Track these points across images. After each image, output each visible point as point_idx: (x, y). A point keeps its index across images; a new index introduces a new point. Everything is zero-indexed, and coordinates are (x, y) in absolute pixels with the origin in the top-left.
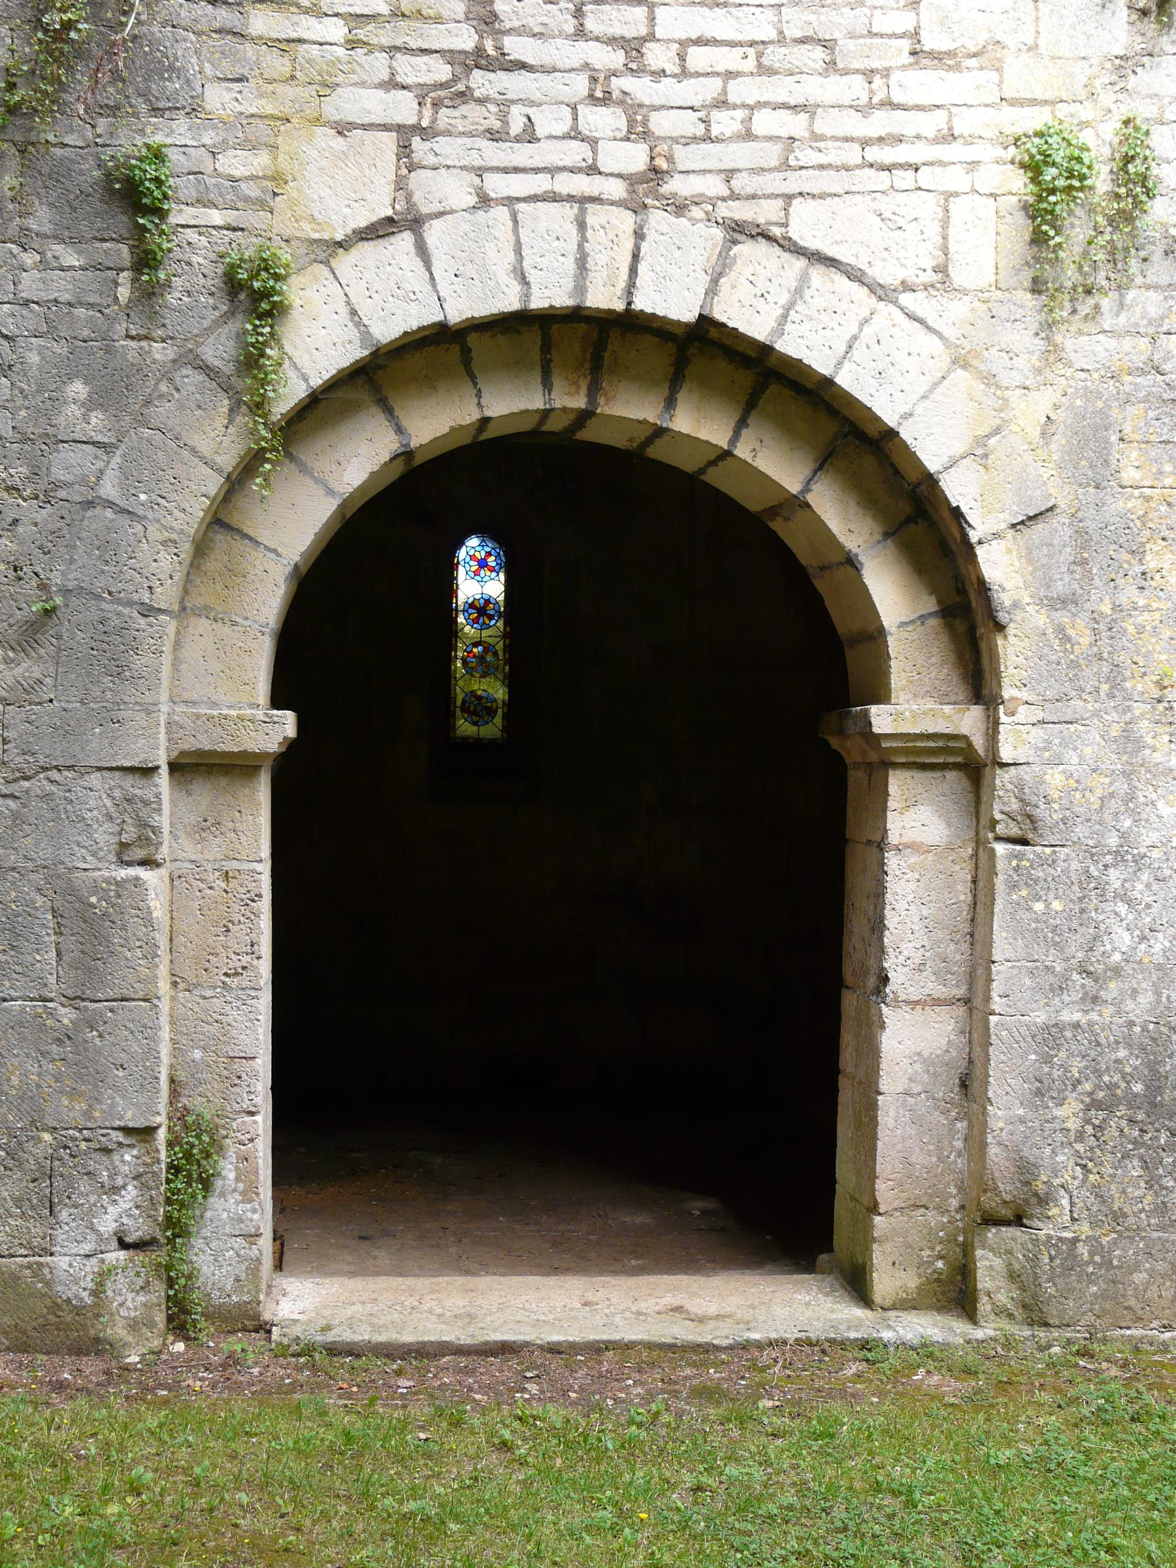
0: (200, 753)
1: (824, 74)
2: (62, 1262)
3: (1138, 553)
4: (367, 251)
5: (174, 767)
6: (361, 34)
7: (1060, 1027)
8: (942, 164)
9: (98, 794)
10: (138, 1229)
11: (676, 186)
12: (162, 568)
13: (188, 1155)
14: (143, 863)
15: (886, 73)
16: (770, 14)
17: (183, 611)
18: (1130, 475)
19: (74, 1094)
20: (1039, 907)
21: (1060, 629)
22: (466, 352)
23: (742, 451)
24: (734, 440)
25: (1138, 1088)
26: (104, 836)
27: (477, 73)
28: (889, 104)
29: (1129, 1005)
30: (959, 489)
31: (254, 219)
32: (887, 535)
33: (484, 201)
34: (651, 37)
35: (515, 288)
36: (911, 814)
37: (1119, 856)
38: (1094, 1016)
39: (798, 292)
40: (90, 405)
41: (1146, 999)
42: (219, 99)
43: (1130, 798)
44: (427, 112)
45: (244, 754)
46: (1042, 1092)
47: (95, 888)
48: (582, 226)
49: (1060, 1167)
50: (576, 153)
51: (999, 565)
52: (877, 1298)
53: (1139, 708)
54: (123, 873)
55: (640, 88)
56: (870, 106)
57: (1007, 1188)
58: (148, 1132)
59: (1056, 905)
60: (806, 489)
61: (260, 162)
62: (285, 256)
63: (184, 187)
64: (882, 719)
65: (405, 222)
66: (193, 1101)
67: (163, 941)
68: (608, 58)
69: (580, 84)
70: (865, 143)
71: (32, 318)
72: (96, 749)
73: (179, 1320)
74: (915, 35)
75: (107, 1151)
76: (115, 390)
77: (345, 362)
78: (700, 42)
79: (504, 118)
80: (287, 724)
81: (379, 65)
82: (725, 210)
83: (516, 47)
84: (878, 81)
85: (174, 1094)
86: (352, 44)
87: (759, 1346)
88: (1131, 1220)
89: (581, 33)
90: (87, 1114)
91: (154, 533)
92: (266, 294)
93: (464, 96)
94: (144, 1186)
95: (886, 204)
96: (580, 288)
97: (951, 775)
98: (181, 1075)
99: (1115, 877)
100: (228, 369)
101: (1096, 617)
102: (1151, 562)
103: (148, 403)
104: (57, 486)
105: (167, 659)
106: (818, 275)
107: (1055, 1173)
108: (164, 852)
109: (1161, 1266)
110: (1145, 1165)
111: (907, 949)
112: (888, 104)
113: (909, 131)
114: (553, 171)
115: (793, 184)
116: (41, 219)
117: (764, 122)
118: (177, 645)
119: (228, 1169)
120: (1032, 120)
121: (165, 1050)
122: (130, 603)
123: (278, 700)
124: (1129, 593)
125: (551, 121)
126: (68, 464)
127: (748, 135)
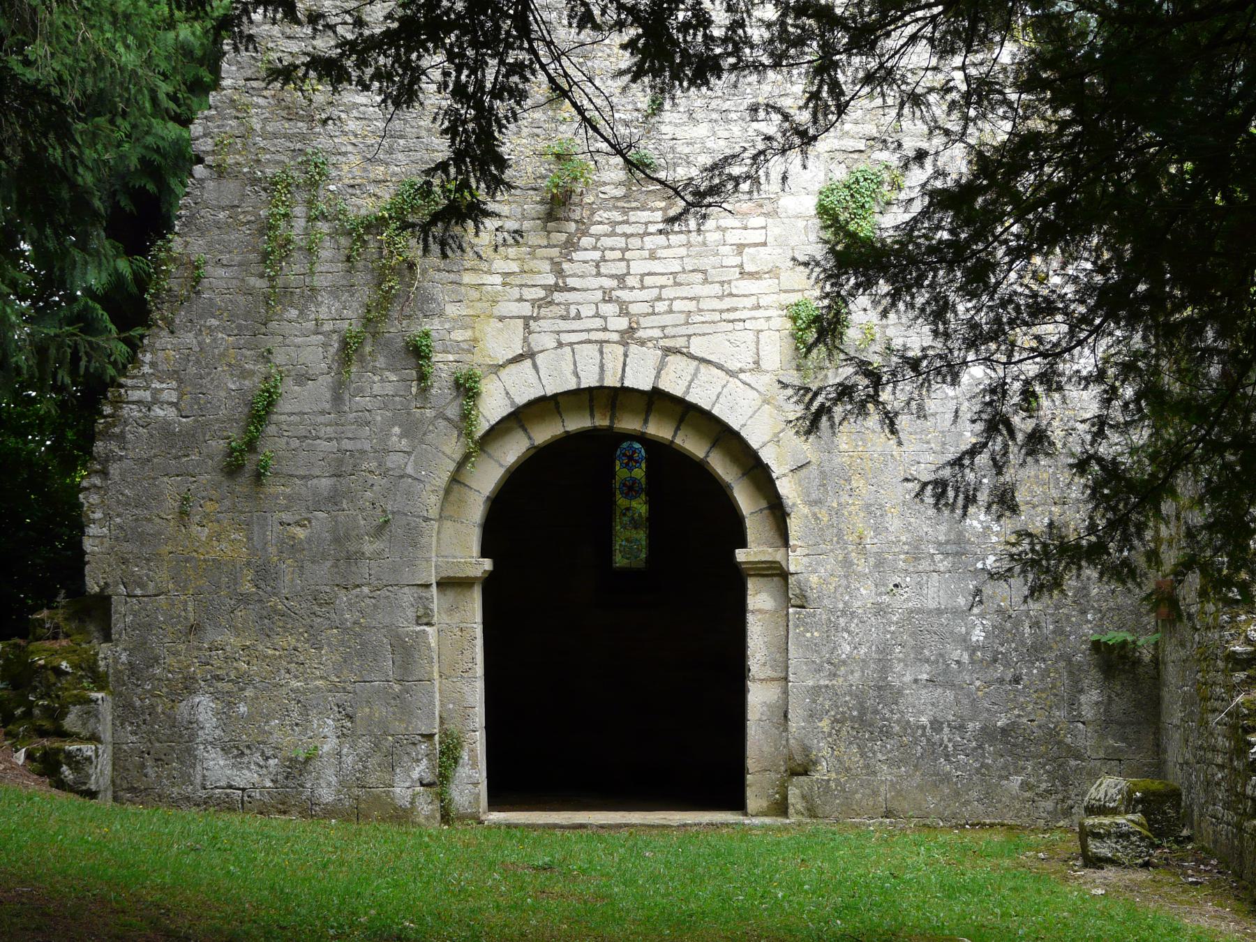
0: (449, 578)
1: (703, 284)
2: (398, 790)
3: (849, 481)
5: (438, 584)
6: (508, 280)
7: (820, 687)
8: (755, 318)
9: (408, 596)
10: (428, 778)
11: (640, 334)
12: (432, 501)
13: (448, 747)
14: (427, 624)
15: (729, 282)
16: (678, 261)
18: (843, 447)
19: (401, 720)
20: (808, 635)
21: (814, 515)
22: (557, 404)
23: (678, 441)
24: (674, 437)
25: (855, 713)
26: (411, 613)
27: (556, 293)
28: (731, 295)
29: (850, 677)
30: (767, 456)
31: (466, 357)
32: (744, 475)
33: (560, 345)
34: (628, 274)
35: (574, 379)
36: (758, 597)
37: (844, 612)
38: (834, 682)
39: (695, 375)
40: (401, 436)
41: (857, 675)
42: (451, 310)
43: (848, 587)
44: (536, 310)
45: (467, 578)
46: (812, 716)
47: (407, 635)
48: (601, 353)
49: (822, 749)
50: (598, 323)
51: (785, 488)
52: (749, 811)
53: (851, 548)
54: (418, 628)
55: (624, 295)
56: (723, 296)
57: (799, 758)
58: (431, 736)
59: (816, 634)
60: (707, 456)
61: (468, 334)
62: (478, 372)
63: (437, 345)
64: (741, 555)
65: (528, 355)
66: (450, 726)
67: (436, 657)
68: (609, 283)
69: (599, 295)
70: (721, 311)
71: (378, 402)
72: (406, 577)
73: (446, 817)
74: (741, 266)
75: (414, 744)
76: (412, 429)
77: (505, 414)
78: (649, 274)
79: (568, 311)
80: (487, 564)
81: (515, 293)
82: (662, 343)
83: (571, 282)
84: (726, 286)
85: (442, 723)
86: (504, 285)
87: (691, 825)
88: (854, 771)
89: (599, 274)
90: (406, 729)
91: (428, 487)
92: (471, 389)
93: (551, 303)
94: (430, 760)
95: (731, 337)
96: (602, 378)
97: (775, 579)
98: (445, 715)
99: (842, 621)
100: (457, 419)
101: (830, 509)
102: (854, 484)
103: (424, 434)
104: (388, 470)
105: (434, 539)
106: (703, 367)
107: (819, 751)
108: (435, 620)
109: (867, 791)
110: (859, 747)
111: (758, 656)
112: (731, 295)
113: (740, 306)
114: (588, 331)
115: (691, 330)
116: (381, 362)
117: (678, 305)
118: (439, 532)
119: (465, 756)
120: (794, 298)
121: (437, 703)
122: (419, 517)
123: (484, 554)
124: (845, 498)
125: (587, 311)
126: (393, 460)
127: (671, 311)
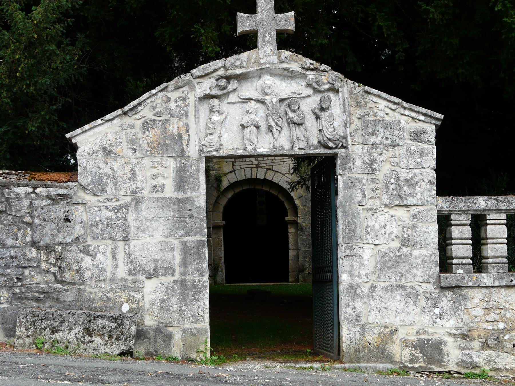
4: (230, 174)
11: (261, 165)
17: (213, 211)
31: (218, 172)
50: (250, 163)
61: (219, 166)
65: (234, 171)
95: (283, 165)
96: (251, 176)
123: (223, 220)
